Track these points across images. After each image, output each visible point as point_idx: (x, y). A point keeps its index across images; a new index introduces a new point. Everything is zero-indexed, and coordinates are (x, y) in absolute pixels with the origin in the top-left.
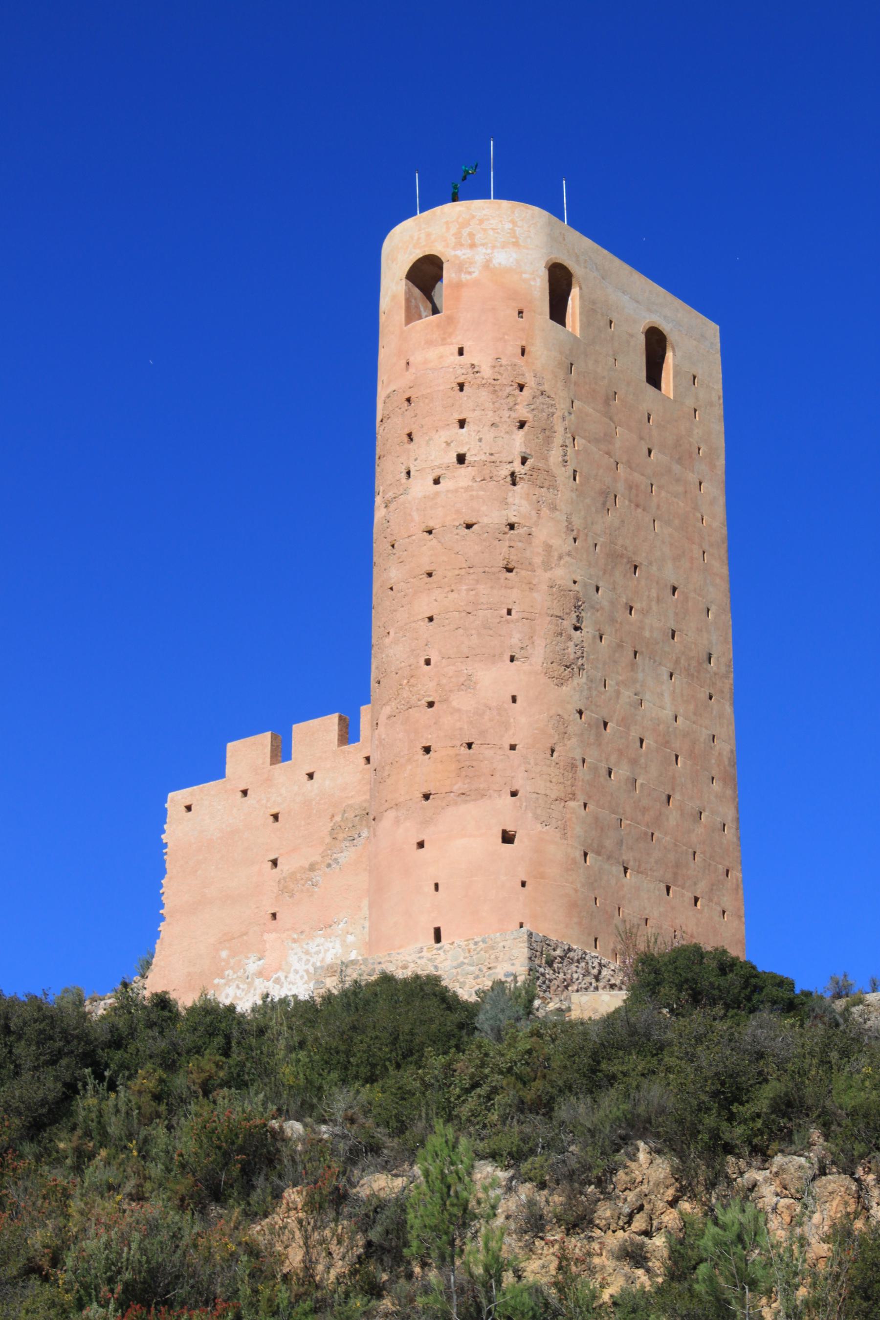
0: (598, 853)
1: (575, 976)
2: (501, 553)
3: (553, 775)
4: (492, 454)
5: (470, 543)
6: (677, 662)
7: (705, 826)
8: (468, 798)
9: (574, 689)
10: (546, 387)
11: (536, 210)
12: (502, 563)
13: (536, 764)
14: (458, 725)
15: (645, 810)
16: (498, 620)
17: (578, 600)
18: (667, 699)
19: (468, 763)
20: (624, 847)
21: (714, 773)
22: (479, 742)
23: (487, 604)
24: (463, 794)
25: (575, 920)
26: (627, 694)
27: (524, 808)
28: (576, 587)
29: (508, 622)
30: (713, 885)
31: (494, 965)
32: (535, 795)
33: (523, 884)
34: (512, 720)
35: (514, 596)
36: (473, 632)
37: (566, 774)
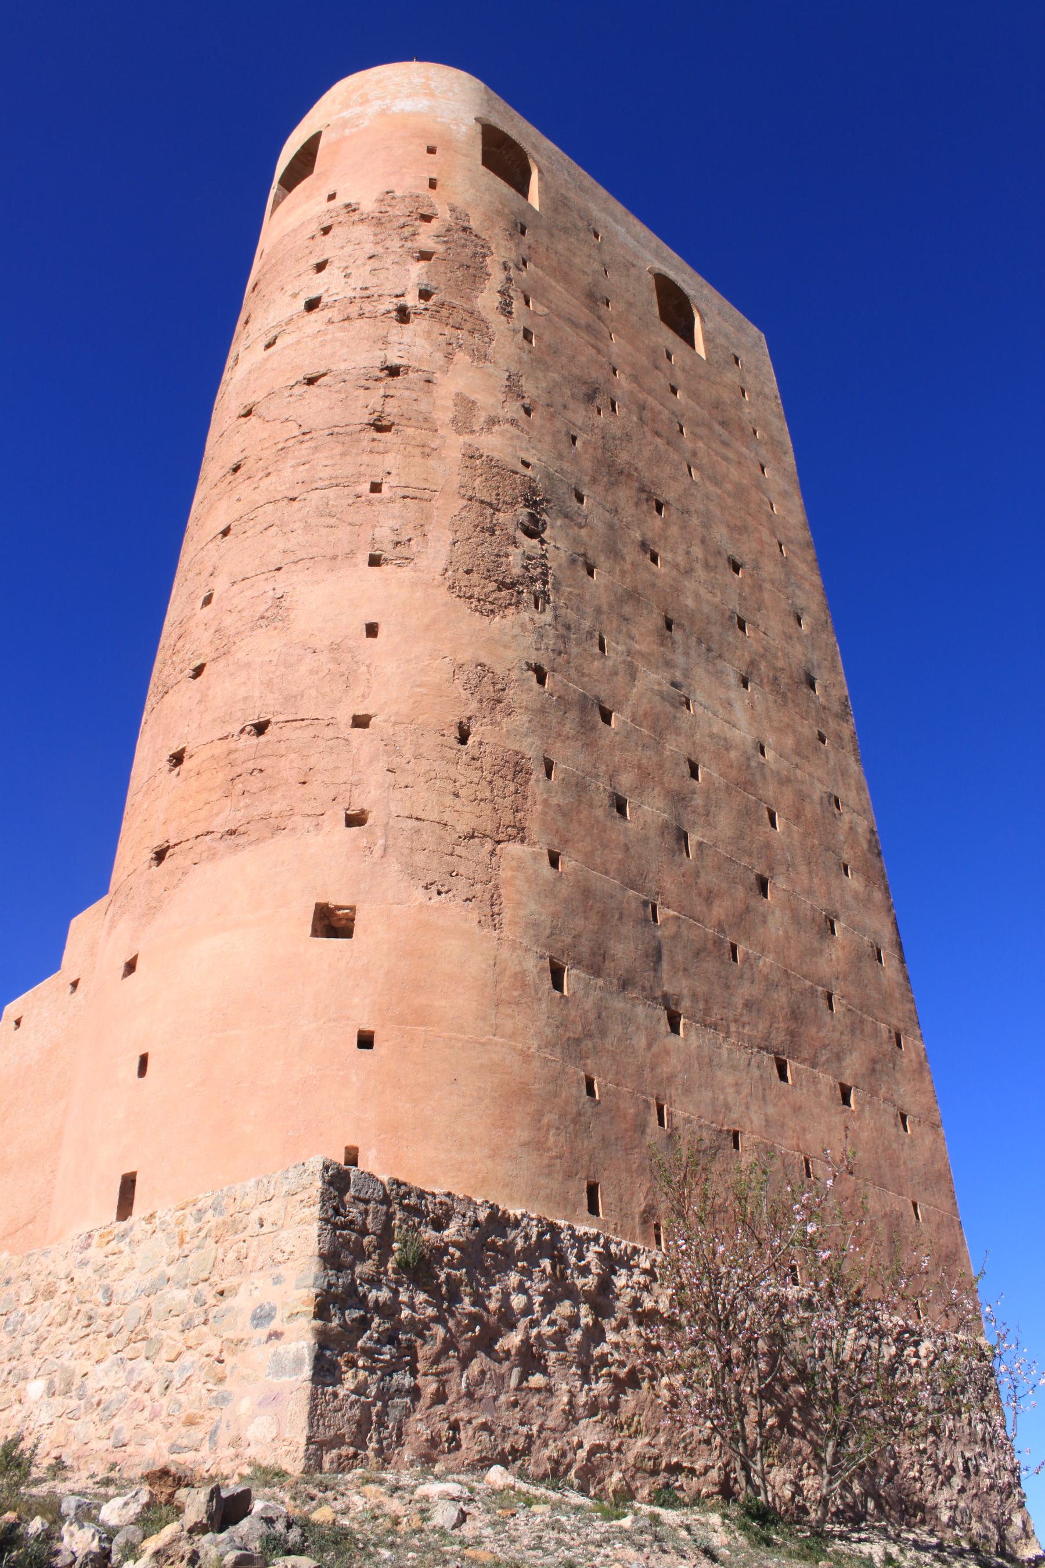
0: (596, 971)
1: (518, 1301)
2: (366, 403)
3: (462, 780)
4: (366, 289)
5: (315, 409)
6: (752, 663)
7: (843, 948)
8: (242, 840)
9: (523, 626)
10: (473, 224)
11: (464, 75)
13: (417, 757)
14: (242, 693)
15: (709, 897)
16: (350, 501)
17: (535, 493)
18: (741, 715)
19: (251, 765)
20: (665, 965)
21: (846, 856)
22: (282, 718)
23: (331, 478)
24: (232, 833)
25: (523, 1135)
26: (651, 679)
27: (378, 851)
28: (529, 472)
29: (370, 503)
30: (874, 1061)
31: (234, 1281)
33: (365, 1041)
34: (363, 669)
35: (391, 459)
36: (296, 526)
37: (499, 782)
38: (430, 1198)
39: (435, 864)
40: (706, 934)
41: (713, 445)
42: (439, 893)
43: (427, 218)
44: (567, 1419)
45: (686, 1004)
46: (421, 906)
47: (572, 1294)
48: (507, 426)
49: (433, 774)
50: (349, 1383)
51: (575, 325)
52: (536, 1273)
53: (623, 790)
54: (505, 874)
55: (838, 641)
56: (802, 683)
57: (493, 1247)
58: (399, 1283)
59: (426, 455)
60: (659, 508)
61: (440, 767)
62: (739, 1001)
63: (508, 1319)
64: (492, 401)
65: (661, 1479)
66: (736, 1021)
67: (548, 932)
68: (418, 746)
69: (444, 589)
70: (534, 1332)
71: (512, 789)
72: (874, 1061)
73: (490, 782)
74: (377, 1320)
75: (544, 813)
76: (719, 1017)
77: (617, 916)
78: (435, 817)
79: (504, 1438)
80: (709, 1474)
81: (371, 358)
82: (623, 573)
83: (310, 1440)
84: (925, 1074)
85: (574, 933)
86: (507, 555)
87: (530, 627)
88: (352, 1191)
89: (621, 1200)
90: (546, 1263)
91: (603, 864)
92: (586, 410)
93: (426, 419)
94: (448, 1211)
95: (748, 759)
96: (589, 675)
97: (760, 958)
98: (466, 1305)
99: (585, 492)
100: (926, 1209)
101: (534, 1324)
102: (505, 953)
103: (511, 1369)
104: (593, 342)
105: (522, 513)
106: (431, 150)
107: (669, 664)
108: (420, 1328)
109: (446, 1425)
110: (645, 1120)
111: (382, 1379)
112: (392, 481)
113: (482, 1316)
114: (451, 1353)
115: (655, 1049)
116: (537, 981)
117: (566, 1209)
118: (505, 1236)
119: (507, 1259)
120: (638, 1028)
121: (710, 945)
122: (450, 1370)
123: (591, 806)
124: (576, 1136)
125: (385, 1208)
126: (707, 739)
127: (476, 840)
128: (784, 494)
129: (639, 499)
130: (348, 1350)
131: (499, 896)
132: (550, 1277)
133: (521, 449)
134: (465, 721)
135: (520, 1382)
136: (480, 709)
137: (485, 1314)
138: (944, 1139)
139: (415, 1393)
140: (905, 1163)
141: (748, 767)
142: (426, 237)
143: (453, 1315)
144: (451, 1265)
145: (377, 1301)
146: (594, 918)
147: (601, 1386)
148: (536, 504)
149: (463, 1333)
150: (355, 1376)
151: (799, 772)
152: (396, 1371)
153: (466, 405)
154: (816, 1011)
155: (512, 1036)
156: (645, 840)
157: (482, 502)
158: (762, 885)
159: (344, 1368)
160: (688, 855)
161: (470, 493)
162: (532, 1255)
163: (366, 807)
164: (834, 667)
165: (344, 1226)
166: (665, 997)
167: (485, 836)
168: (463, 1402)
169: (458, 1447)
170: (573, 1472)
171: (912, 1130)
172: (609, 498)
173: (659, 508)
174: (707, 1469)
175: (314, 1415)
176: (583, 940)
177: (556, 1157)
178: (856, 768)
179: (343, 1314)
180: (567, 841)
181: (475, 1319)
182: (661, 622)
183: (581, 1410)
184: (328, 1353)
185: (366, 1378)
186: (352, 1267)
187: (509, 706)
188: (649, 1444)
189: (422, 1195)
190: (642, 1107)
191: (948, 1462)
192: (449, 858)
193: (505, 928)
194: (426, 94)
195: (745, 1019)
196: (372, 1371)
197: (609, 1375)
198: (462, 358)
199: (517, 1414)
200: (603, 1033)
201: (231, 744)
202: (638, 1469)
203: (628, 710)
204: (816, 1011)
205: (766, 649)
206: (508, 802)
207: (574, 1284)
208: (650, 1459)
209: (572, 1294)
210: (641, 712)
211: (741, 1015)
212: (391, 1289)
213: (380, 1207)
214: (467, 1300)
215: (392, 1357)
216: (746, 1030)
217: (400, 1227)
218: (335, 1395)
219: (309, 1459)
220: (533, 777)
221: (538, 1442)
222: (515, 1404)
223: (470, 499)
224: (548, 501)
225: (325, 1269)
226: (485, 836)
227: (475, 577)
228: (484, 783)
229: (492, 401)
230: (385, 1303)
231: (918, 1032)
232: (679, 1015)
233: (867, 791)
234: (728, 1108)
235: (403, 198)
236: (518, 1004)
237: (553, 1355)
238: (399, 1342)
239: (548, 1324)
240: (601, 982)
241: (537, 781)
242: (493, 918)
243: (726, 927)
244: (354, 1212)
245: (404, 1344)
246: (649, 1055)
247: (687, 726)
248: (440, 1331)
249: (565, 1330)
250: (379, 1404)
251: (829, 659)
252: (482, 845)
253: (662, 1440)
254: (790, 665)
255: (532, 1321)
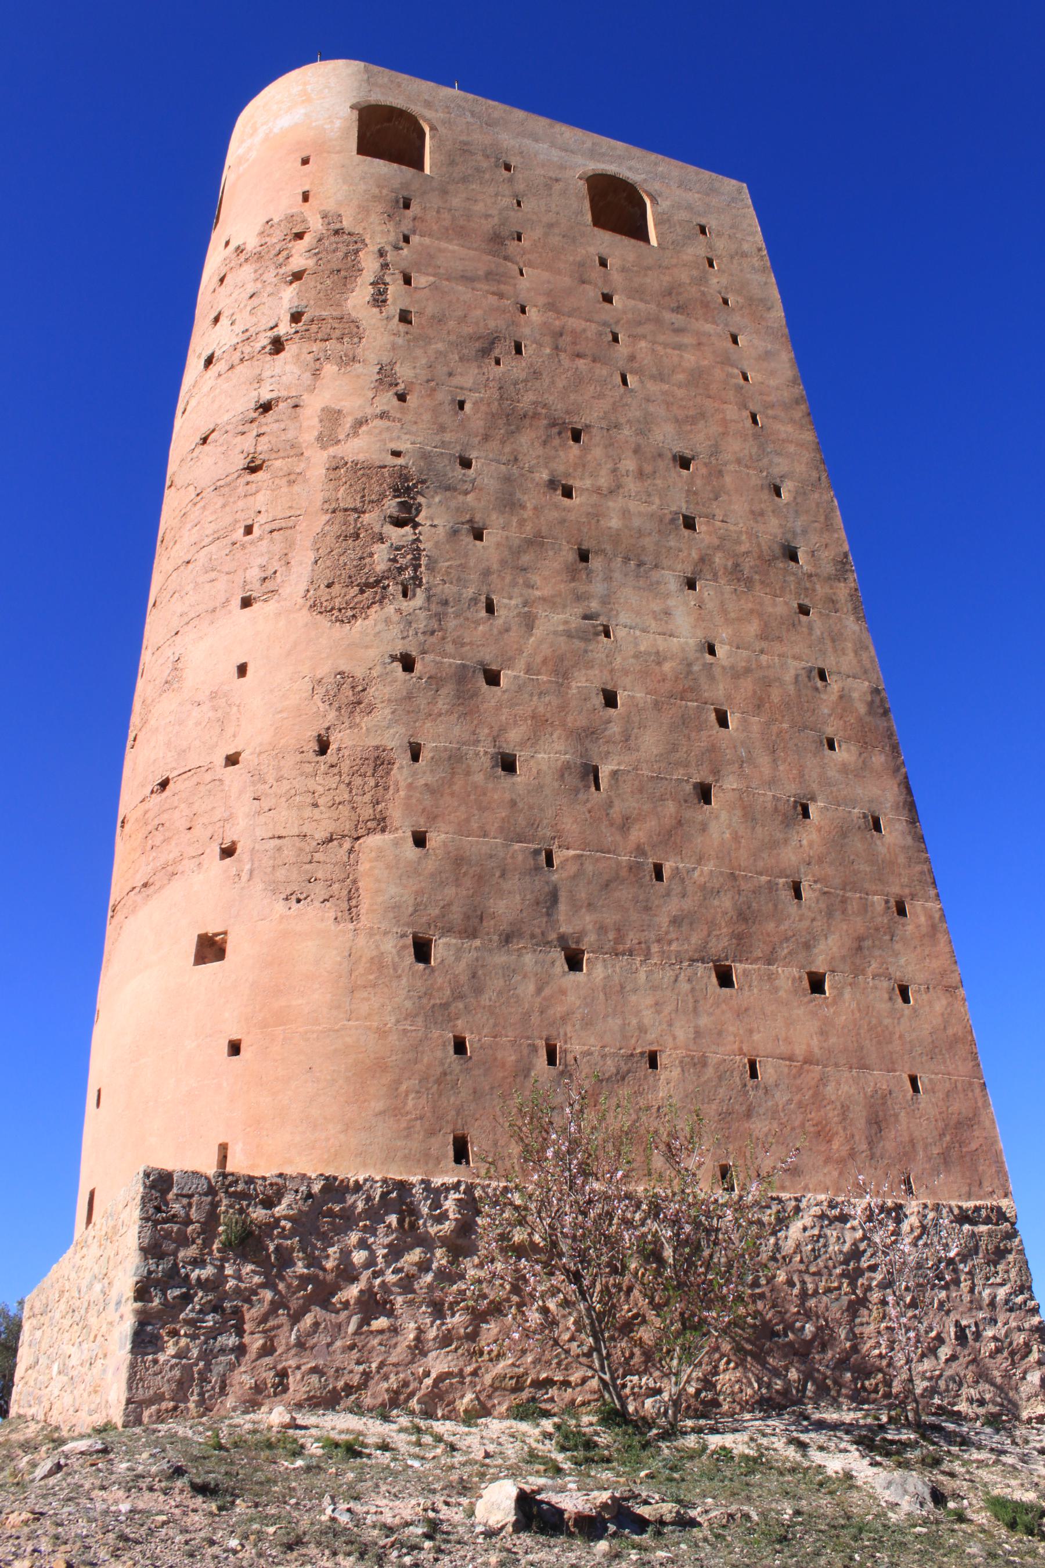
1: (359, 1257)
7: (819, 830)
8: (152, 889)
10: (346, 224)
11: (340, 63)
12: (242, 463)
15: (625, 825)
19: (156, 822)
27: (245, 876)
28: (400, 461)
32: (277, 842)
33: (235, 1048)
34: (235, 709)
37: (358, 781)
38: (260, 1182)
39: (294, 876)
40: (619, 863)
41: (661, 338)
42: (299, 901)
43: (299, 236)
44: (413, 1354)
45: (590, 939)
46: (282, 917)
47: (426, 1243)
48: (378, 422)
49: (293, 792)
50: (171, 1350)
51: (467, 279)
52: (381, 1229)
53: (512, 746)
54: (363, 867)
55: (836, 495)
56: (775, 558)
57: (330, 1213)
58: (224, 1260)
59: (292, 483)
60: (576, 436)
61: (300, 783)
62: (663, 920)
63: (347, 1273)
64: (358, 402)
65: (525, 1395)
66: (658, 941)
67: (411, 909)
68: (279, 769)
69: (305, 611)
70: (378, 1281)
71: (372, 783)
72: (860, 939)
73: (349, 784)
74: (200, 1294)
75: (409, 797)
76: (635, 941)
77: (498, 874)
78: (296, 831)
79: (337, 1378)
80: (588, 1383)
81: (245, 403)
82: (522, 523)
83: (129, 1402)
84: (940, 936)
85: (442, 903)
86: (371, 555)
87: (396, 618)
88: (175, 1190)
89: (496, 1144)
90: (393, 1219)
91: (481, 828)
92: (480, 367)
93: (293, 446)
94: (279, 1190)
95: (690, 665)
96: (471, 643)
97: (694, 869)
98: (300, 1268)
99: (473, 455)
100: (931, 1080)
101: (376, 1274)
102: (361, 941)
103: (350, 1317)
104: (494, 289)
105: (391, 505)
106: (305, 161)
107: (579, 598)
108: (248, 1296)
109: (272, 1373)
110: (531, 1063)
111: (206, 1342)
112: (262, 519)
113: (317, 1276)
114: (281, 1312)
115: (547, 991)
116: (397, 959)
117: (427, 1163)
118: (344, 1201)
119: (347, 1220)
120: (525, 977)
121: (624, 873)
122: (279, 1327)
123: (468, 773)
124: (440, 1095)
125: (209, 1198)
126: (632, 661)
127: (335, 842)
128: (767, 355)
129: (549, 436)
130: (172, 1322)
131: (357, 890)
132: (396, 1230)
133: (391, 440)
134: (323, 732)
135: (360, 1326)
136: (338, 718)
137: (321, 1273)
138: (964, 1000)
139: (241, 1350)
140: (901, 1037)
141: (689, 673)
142: (300, 258)
143: (283, 1279)
144: (282, 1236)
145: (199, 1279)
146: (468, 882)
147: (457, 1320)
148: (408, 489)
149: (294, 1293)
150: (177, 1343)
151: (764, 658)
152: (221, 1334)
153: (332, 416)
154: (776, 906)
155: (368, 1017)
156: (540, 788)
157: (346, 510)
158: (704, 794)
159: (166, 1338)
160: (598, 788)
161: (334, 505)
162: (375, 1214)
163: (235, 838)
164: (828, 526)
165: (166, 1221)
166: (562, 939)
167: (344, 836)
168: (293, 1351)
169: (286, 1390)
170: (416, 1399)
171: (916, 1000)
172: (507, 450)
173: (576, 436)
174: (584, 1380)
175: (133, 1380)
176: (455, 908)
177: (416, 1119)
178: (856, 628)
179: (165, 1294)
180: (435, 817)
181: (304, 1280)
182: (571, 556)
183: (431, 1343)
184: (149, 1328)
185: (188, 1344)
186: (175, 1253)
187: (370, 705)
188: (513, 1365)
189: (250, 1180)
190: (525, 1052)
191: (933, 1334)
192: (308, 866)
193: (363, 918)
194: (303, 102)
195: (672, 936)
196: (194, 1337)
197: (468, 1308)
198: (330, 369)
199: (355, 1354)
200: (478, 991)
201: (146, 805)
202: (496, 1389)
203: (521, 664)
204: (776, 906)
205: (722, 538)
206: (367, 798)
207: (427, 1232)
208: (511, 1378)
209: (426, 1243)
210: (539, 659)
211: (667, 933)
212: (215, 1266)
213: (204, 1198)
214: (300, 1264)
215: (215, 1323)
216: (674, 947)
217: (226, 1212)
218: (155, 1362)
219: (128, 1416)
220: (396, 766)
221: (377, 1377)
222: (352, 1347)
223: (334, 512)
224: (423, 482)
225: (146, 1259)
226: (344, 836)
227: (337, 589)
228: (342, 786)
229: (358, 402)
230: (207, 1280)
231: (932, 892)
232: (583, 952)
233: (872, 649)
234: (642, 1029)
235: (279, 224)
236: (374, 986)
237: (400, 1299)
238: (223, 1310)
239: (393, 1272)
240: (477, 943)
241: (401, 768)
242: (351, 913)
243: (647, 848)
244: (176, 1208)
245: (229, 1311)
246: (539, 1000)
247: (603, 656)
248: (268, 1295)
249: (413, 1276)
250: (201, 1364)
251: (822, 519)
252: (341, 846)
253: (529, 1360)
254: (759, 545)
255: (374, 1272)
